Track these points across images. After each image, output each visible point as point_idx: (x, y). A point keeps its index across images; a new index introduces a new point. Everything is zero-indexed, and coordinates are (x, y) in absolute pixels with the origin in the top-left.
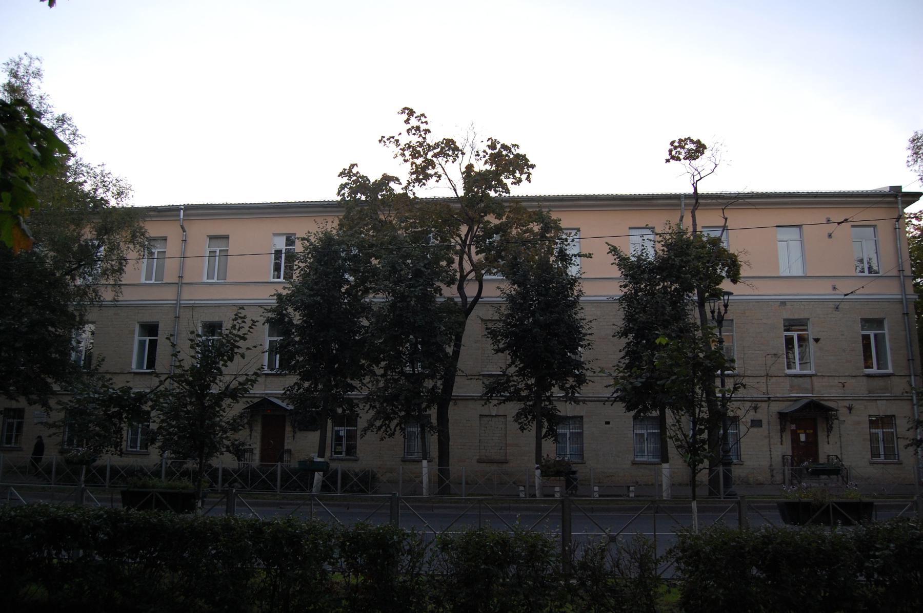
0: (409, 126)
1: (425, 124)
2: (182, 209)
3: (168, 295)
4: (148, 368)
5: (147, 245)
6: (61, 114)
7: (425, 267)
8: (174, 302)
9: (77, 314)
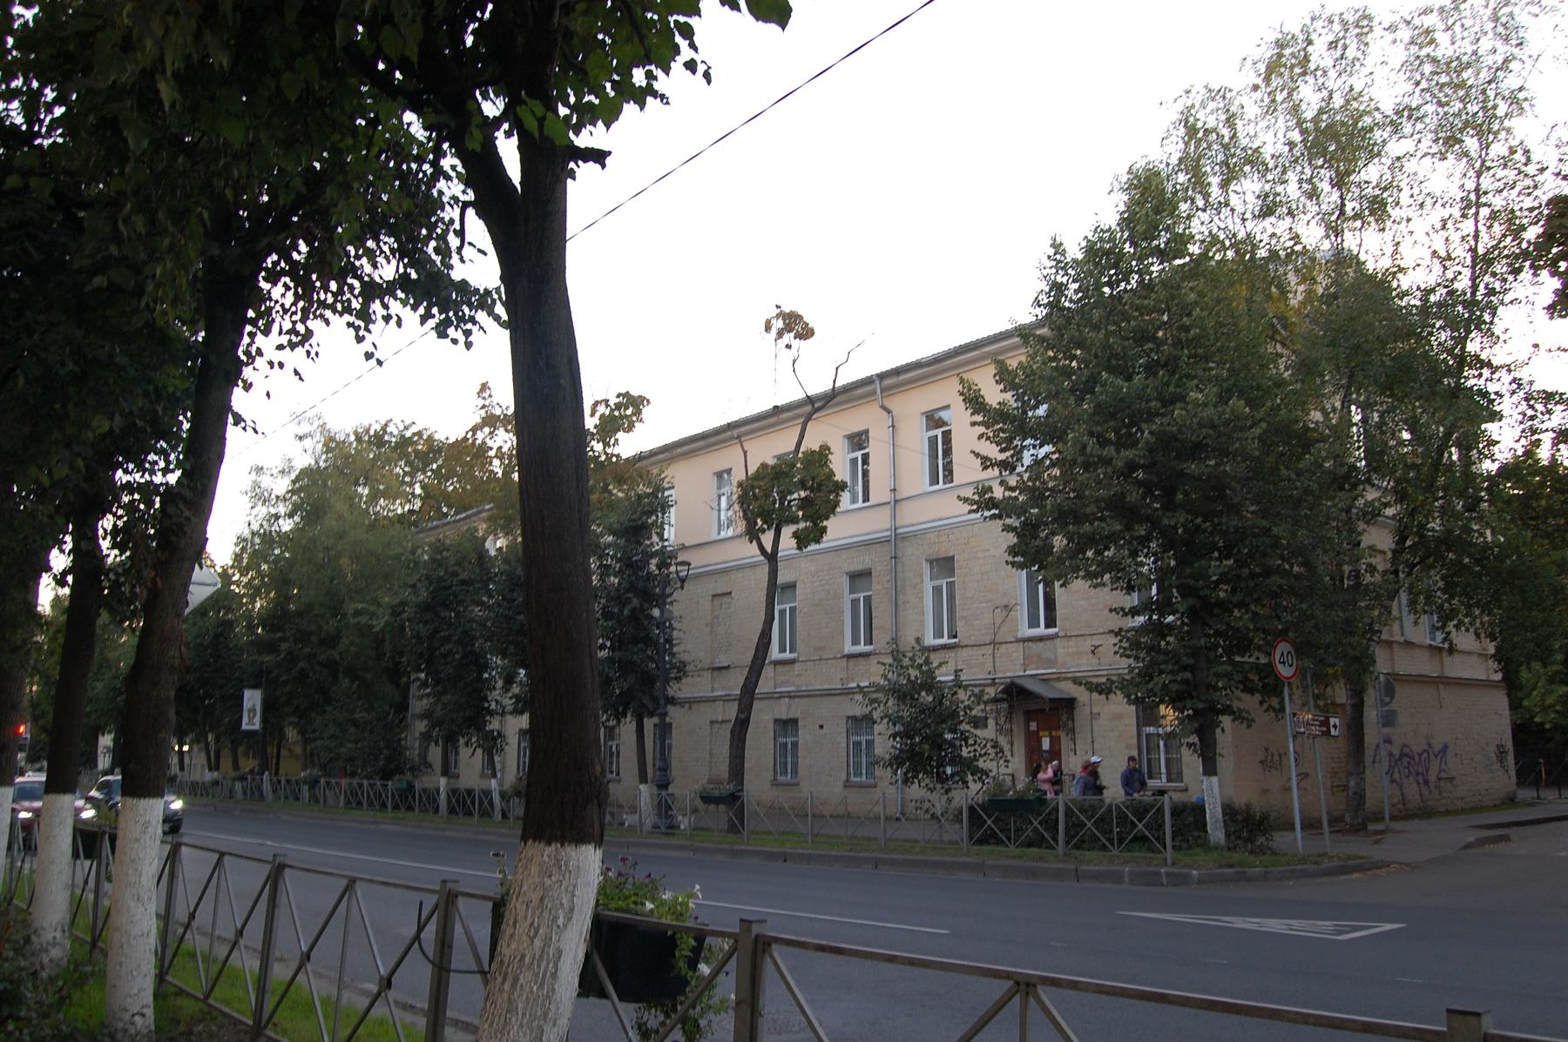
7: (1177, 386)
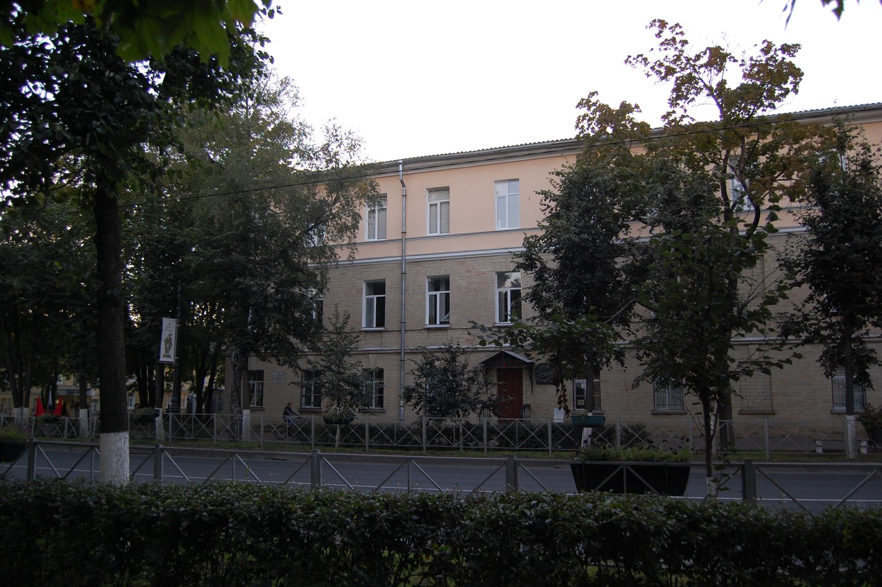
0: (661, 40)
1: (680, 35)
2: (400, 163)
3: (392, 252)
4: (377, 326)
5: (377, 200)
6: (284, 77)
8: (400, 258)
9: (317, 272)
